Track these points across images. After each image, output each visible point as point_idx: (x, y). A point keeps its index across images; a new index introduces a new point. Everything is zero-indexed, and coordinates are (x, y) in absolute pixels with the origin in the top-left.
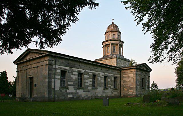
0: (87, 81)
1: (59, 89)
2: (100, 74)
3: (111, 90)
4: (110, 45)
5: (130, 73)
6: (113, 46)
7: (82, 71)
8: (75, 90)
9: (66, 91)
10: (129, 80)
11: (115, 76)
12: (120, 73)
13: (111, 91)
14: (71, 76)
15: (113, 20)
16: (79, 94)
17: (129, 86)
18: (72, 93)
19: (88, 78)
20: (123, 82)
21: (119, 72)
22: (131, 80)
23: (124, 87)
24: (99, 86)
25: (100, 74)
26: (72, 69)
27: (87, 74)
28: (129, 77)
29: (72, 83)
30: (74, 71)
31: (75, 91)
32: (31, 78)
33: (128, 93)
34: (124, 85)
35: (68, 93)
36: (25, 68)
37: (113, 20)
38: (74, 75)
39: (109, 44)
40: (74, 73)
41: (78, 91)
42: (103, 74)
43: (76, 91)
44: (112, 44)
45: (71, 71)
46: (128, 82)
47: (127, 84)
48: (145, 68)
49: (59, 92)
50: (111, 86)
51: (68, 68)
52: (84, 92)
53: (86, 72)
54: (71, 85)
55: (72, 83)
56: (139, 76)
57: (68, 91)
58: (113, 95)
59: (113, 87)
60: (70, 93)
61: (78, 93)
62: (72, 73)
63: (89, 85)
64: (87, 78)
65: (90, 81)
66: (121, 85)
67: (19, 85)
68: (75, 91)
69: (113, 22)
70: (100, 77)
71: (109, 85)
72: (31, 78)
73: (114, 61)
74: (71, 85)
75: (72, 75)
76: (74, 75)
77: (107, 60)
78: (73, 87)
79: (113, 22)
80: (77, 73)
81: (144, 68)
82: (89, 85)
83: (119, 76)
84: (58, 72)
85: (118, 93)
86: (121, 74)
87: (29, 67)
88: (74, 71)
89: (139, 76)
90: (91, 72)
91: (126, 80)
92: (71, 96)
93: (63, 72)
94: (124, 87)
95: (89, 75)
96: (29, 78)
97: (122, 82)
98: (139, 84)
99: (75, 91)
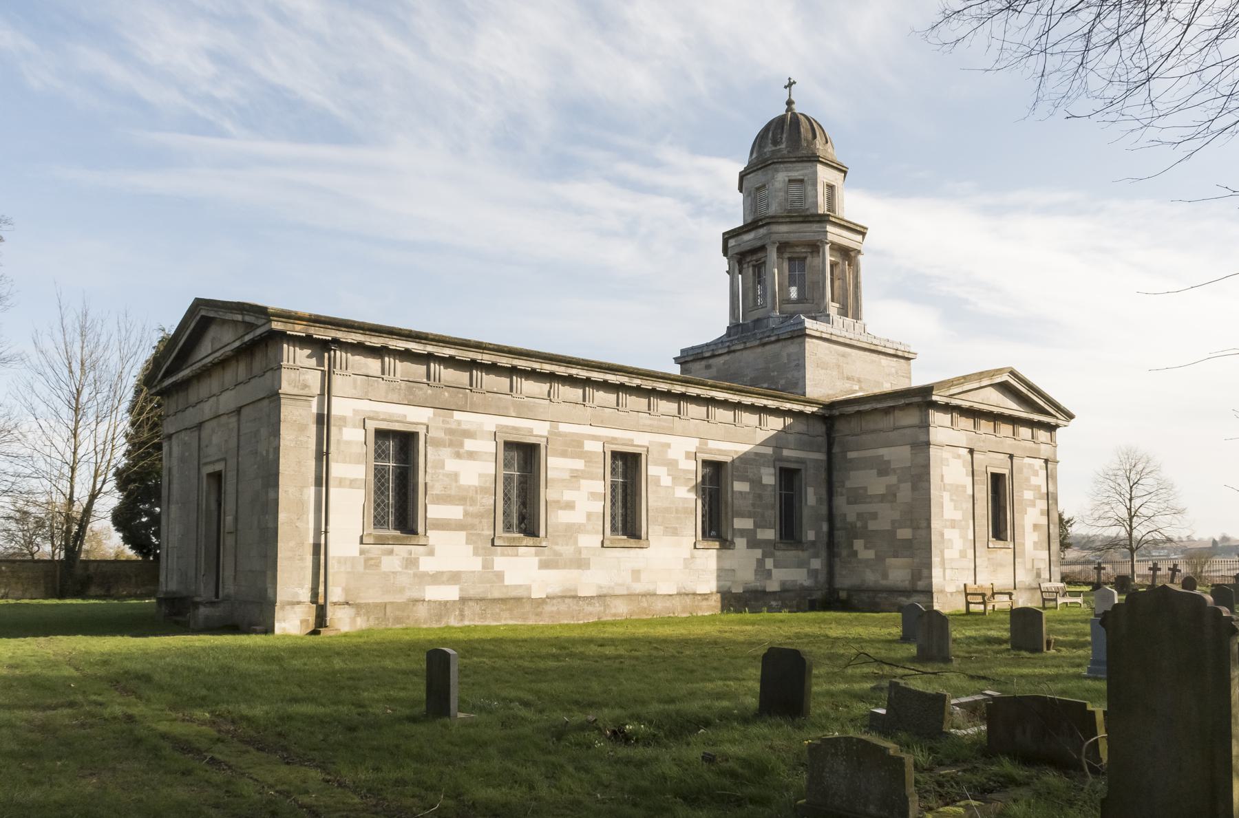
0: (568, 495)
1: (362, 552)
2: (669, 446)
3: (758, 553)
4: (773, 254)
5: (893, 435)
6: (790, 259)
7: (531, 430)
8: (476, 553)
9: (411, 562)
10: (888, 487)
11: (788, 460)
12: (822, 440)
13: (760, 562)
14: (451, 465)
15: (790, 84)
16: (506, 583)
17: (887, 526)
18: (454, 578)
19: (576, 476)
20: (849, 503)
21: (842, 427)
22: (902, 485)
23: (853, 533)
24: (875, 472)
25: (669, 446)
26: (459, 423)
27: (574, 447)
28: (883, 469)
29: (454, 512)
30: (469, 434)
31: (479, 560)
32: (217, 477)
33: (885, 576)
34: (851, 518)
35: (425, 574)
36: (191, 417)
37: (790, 84)
38: (472, 455)
39: (763, 248)
40: (469, 445)
41: (501, 562)
42: (692, 444)
43: (487, 565)
44: (783, 247)
45: (450, 432)
46: (882, 498)
47: (874, 516)
48: (1015, 406)
49: (361, 568)
50: (756, 525)
51: (430, 412)
52: (544, 565)
53: (560, 434)
54: (443, 525)
55: (454, 512)
56: (959, 456)
57: (427, 565)
58: (773, 586)
59: (769, 534)
60: (436, 578)
61: (500, 576)
62: (451, 444)
63: (583, 520)
64: (566, 476)
65: (593, 495)
66: (838, 524)
67: (172, 516)
68: (476, 564)
69: (790, 103)
70: (672, 465)
71: (739, 523)
72: (217, 477)
73: (789, 355)
74: (443, 525)
75: (458, 455)
76: (472, 455)
77: (746, 353)
78: (463, 534)
79: (790, 103)
80: (490, 447)
81: (1010, 407)
82: (583, 520)
83: (821, 456)
84: (348, 443)
85: (813, 573)
86: (836, 449)
87: (207, 409)
88: (469, 434)
89: (959, 456)
90: (595, 438)
91: (865, 489)
92: (451, 593)
93: (399, 448)
94: (853, 533)
95: (581, 454)
96: (209, 475)
97: (840, 501)
98: (958, 516)
99: (479, 560)
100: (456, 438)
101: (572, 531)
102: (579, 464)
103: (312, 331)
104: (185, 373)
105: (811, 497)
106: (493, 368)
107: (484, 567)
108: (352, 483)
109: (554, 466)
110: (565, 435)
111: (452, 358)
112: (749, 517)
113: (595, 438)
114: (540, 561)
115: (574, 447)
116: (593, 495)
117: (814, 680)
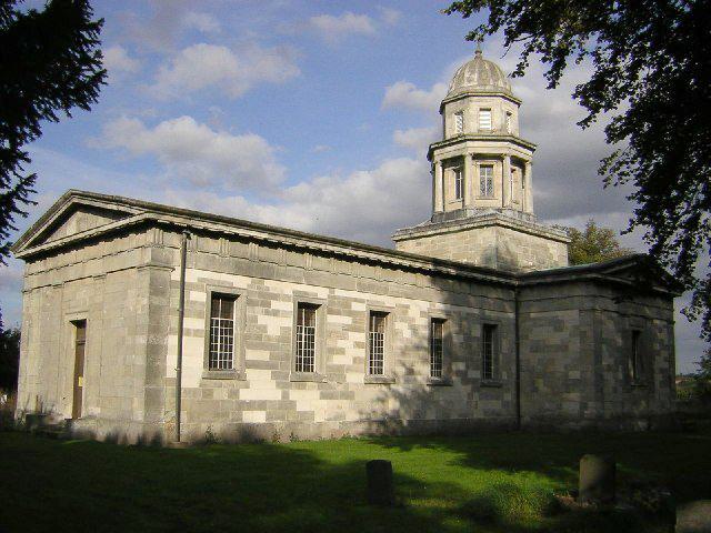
0: (341, 344)
9: (234, 393)
18: (261, 405)
19: (348, 328)
25: (408, 307)
27: (344, 307)
29: (264, 356)
30: (276, 297)
31: (280, 391)
38: (276, 313)
40: (275, 305)
41: (294, 394)
43: (285, 395)
52: (323, 396)
55: (264, 356)
57: (245, 395)
60: (251, 406)
61: (293, 404)
62: (263, 304)
65: (358, 345)
75: (267, 313)
76: (276, 313)
85: (506, 404)
88: (276, 297)
90: (362, 301)
95: (350, 313)
100: (265, 300)
101: (339, 372)
102: (348, 320)
103: (309, 244)
104: (45, 247)
105: (505, 344)
106: (204, 233)
107: (283, 397)
108: (197, 333)
109: (325, 321)
110: (339, 297)
111: (538, 284)
112: (462, 361)
113: (362, 301)
114: (322, 393)
115: (344, 307)
116: (358, 345)
117: (165, 420)
